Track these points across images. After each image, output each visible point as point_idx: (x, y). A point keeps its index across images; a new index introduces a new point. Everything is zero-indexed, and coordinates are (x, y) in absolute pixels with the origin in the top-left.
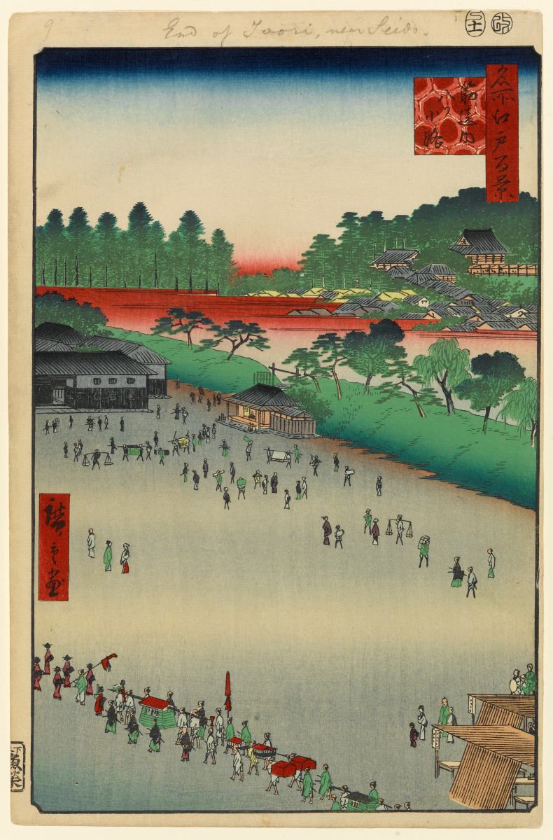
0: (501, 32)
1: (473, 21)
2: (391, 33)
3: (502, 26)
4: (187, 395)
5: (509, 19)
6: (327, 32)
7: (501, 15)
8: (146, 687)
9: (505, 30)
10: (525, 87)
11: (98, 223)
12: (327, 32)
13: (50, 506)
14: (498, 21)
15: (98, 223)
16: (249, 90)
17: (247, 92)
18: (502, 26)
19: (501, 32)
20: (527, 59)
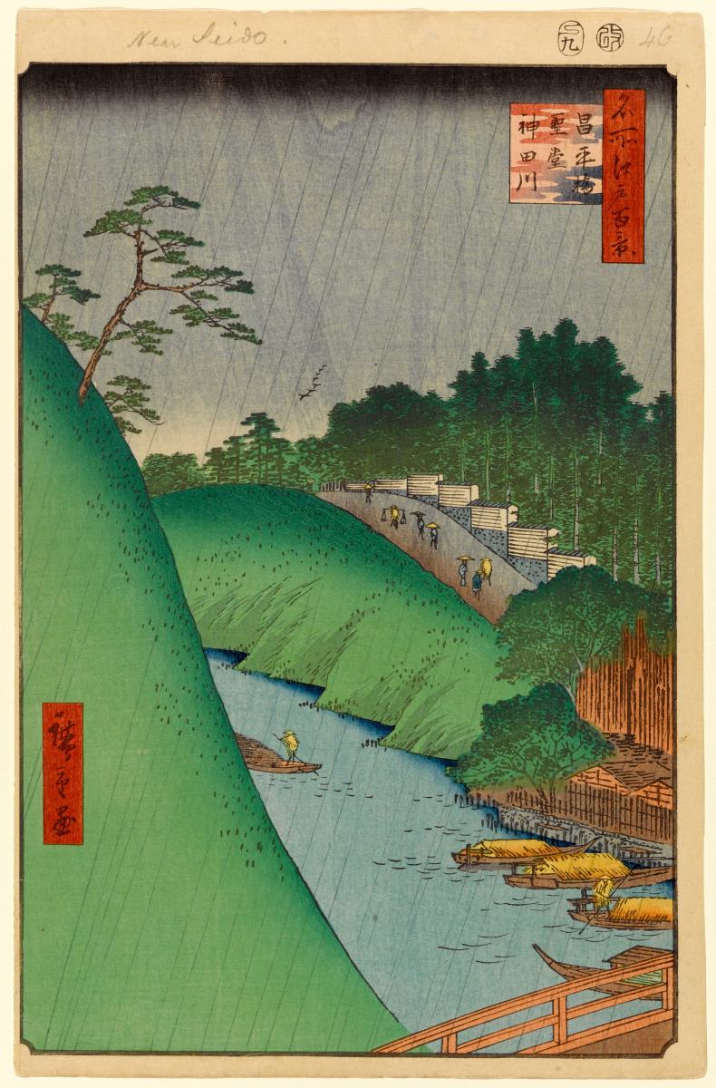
0: (609, 49)
1: (568, 28)
2: (223, 44)
3: (611, 40)
4: (443, 546)
5: (620, 32)
6: (149, 32)
7: (609, 27)
8: (263, 850)
9: (616, 45)
10: (655, 118)
11: (550, 331)
12: (149, 32)
13: (56, 726)
14: (607, 35)
15: (550, 331)
16: (275, 100)
17: (259, 106)
18: (611, 40)
19: (609, 49)
20: (659, 81)
